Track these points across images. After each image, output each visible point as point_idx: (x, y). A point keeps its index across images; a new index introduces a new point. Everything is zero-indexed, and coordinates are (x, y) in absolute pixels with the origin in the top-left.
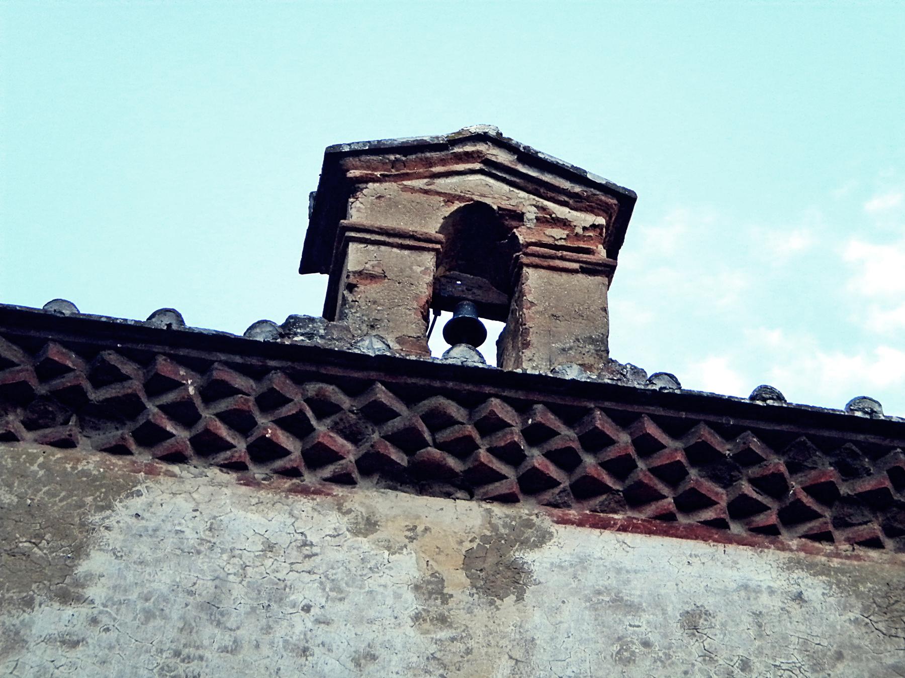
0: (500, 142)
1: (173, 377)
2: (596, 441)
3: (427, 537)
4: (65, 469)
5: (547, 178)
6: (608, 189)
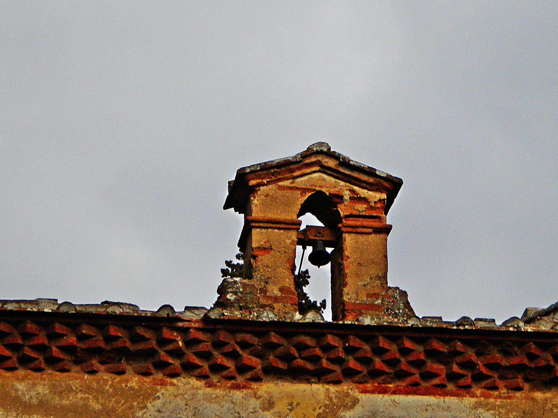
1: (170, 337)
2: (379, 351)
3: (299, 408)
4: (122, 386)
5: (355, 174)
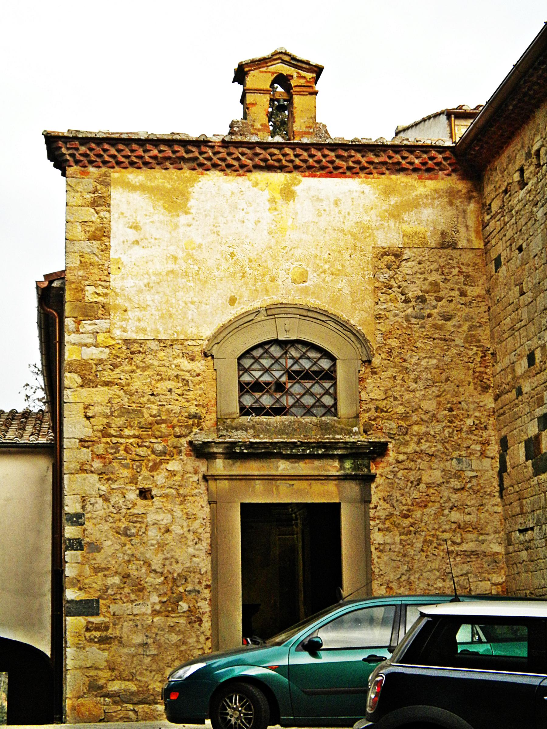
0: (286, 54)
5: (299, 64)
6: (316, 66)
